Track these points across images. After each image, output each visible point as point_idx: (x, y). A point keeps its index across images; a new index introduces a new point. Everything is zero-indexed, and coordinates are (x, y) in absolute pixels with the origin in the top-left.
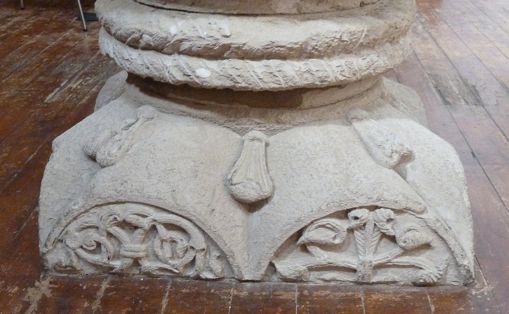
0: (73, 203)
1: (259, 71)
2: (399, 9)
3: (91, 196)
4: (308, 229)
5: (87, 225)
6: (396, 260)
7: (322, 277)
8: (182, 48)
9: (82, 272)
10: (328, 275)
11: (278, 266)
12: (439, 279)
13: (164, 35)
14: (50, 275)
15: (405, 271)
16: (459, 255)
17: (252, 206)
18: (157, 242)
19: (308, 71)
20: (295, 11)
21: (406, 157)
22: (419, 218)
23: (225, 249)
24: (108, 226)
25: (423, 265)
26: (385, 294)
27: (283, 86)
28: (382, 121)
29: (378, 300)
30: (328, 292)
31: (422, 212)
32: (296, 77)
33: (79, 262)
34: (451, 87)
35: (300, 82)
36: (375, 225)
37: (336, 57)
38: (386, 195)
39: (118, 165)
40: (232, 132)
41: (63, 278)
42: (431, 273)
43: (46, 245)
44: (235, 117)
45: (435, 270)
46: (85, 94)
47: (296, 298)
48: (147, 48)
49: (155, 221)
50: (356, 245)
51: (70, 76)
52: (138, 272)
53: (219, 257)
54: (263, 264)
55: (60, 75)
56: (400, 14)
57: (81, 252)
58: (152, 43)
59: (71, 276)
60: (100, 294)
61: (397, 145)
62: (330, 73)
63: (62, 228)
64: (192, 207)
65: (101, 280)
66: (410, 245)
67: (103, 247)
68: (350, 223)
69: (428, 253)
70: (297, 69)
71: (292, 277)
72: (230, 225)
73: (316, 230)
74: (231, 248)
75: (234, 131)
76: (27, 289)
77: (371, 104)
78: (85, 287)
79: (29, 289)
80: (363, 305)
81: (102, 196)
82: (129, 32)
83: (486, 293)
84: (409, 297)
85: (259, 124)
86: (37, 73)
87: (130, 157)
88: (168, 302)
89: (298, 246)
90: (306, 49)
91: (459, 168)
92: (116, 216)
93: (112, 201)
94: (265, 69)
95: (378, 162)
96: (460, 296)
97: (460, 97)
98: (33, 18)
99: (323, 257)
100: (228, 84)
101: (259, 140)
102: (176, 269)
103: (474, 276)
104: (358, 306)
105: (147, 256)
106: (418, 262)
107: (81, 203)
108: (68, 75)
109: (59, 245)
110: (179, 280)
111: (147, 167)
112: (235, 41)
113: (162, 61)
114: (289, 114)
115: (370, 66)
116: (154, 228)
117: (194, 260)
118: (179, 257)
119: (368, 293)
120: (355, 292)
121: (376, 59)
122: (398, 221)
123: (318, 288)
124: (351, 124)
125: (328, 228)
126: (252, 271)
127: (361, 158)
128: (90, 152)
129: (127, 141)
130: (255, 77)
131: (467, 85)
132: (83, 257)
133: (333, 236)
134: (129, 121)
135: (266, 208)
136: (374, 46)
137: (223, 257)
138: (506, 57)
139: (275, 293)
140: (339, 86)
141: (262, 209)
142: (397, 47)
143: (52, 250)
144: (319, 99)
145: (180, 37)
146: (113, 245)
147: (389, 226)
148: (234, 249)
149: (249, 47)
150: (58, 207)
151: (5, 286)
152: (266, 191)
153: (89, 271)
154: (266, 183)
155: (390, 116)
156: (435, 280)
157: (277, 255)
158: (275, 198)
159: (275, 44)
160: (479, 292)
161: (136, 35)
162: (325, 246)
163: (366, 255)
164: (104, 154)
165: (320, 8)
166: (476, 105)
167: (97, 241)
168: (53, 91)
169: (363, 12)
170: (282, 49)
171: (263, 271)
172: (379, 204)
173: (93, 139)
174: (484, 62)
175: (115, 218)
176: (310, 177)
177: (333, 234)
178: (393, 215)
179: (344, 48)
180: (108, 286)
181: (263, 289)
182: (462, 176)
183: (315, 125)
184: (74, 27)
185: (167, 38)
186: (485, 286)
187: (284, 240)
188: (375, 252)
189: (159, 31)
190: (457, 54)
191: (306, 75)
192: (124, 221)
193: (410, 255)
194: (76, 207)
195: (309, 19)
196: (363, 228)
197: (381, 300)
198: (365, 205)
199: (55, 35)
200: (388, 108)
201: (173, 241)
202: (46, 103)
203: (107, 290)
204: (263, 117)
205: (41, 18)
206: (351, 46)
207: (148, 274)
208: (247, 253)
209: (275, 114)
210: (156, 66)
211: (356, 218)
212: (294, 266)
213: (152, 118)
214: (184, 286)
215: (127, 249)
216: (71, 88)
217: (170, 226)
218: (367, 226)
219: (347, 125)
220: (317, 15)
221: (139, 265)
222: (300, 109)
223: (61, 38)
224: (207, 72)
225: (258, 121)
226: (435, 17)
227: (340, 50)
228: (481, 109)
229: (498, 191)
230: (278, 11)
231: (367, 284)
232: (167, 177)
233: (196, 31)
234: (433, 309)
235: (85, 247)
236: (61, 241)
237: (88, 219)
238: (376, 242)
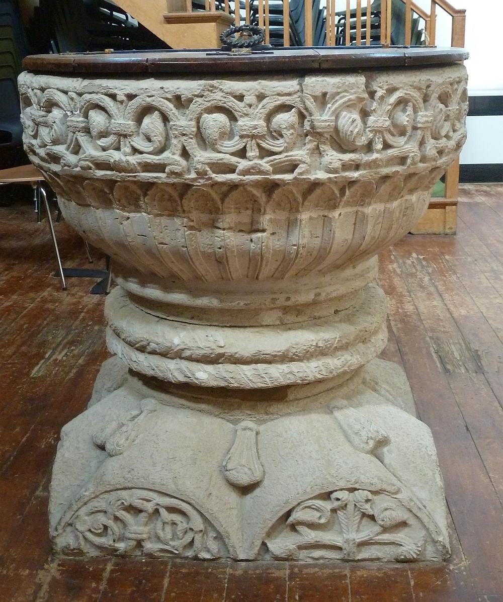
0: (84, 489)
1: (249, 374)
2: (369, 314)
3: (101, 483)
4: (295, 510)
5: (96, 509)
6: (377, 538)
7: (311, 556)
8: (183, 355)
9: (88, 554)
10: (317, 553)
11: (269, 545)
12: (418, 555)
14: (58, 558)
15: (387, 548)
16: (434, 532)
17: (245, 490)
18: (159, 524)
19: (291, 373)
20: (278, 322)
21: (382, 442)
22: (393, 498)
23: (221, 530)
24: (116, 510)
25: (403, 542)
26: (369, 570)
27: (270, 385)
28: (360, 408)
29: (362, 576)
30: (317, 569)
31: (396, 493)
32: (281, 377)
33: (85, 544)
34: (453, 352)
35: (284, 381)
36: (355, 505)
37: (315, 359)
38: (363, 478)
39: (125, 454)
40: (226, 422)
41: (71, 560)
42: (410, 549)
43: (56, 529)
44: (229, 409)
45: (414, 547)
46: (72, 367)
47: (287, 575)
48: (153, 353)
49: (158, 504)
50: (340, 524)
51: (54, 345)
52: (140, 554)
53: (215, 538)
54: (256, 544)
55: (43, 344)
56: (369, 318)
57: (89, 536)
58: (157, 350)
59: (77, 558)
60: (106, 575)
61: (372, 431)
62: (309, 373)
63: (73, 513)
64: (191, 492)
65: (105, 562)
66: (388, 523)
67: (109, 529)
68: (333, 503)
69: (406, 530)
70: (281, 371)
71: (283, 555)
72: (226, 509)
73: (303, 511)
74: (227, 529)
75: (228, 421)
76: (37, 571)
77: (352, 392)
78: (91, 569)
79: (39, 571)
80: (348, 581)
81: (112, 483)
82: (138, 340)
83: (463, 568)
84: (392, 573)
85: (250, 415)
86: (19, 342)
87: (136, 447)
88: (170, 581)
89: (287, 526)
90: (288, 355)
91: (432, 450)
92: (123, 501)
93: (120, 487)
94: (253, 372)
95: (356, 448)
96: (440, 572)
97: (461, 363)
98: (6, 273)
99: (311, 536)
100: (222, 384)
101: (250, 429)
102: (176, 550)
103: (450, 552)
104: (344, 582)
105: (149, 538)
106: (397, 539)
107: (92, 490)
108: (51, 344)
109: (69, 529)
110: (178, 561)
111: (151, 456)
112: (229, 350)
113: (166, 364)
114: (276, 405)
115: (345, 365)
116: (157, 511)
117: (192, 541)
118: (178, 539)
119: (353, 570)
120: (341, 569)
121: (349, 358)
122: (376, 501)
123: (307, 566)
124: (332, 412)
125: (314, 509)
126: (247, 551)
127: (341, 444)
128: (99, 442)
129: (133, 432)
130: (246, 379)
131: (469, 349)
132: (90, 540)
133: (319, 516)
134: (135, 413)
135: (257, 492)
136: (347, 347)
137: (219, 537)
139: (268, 572)
140: (320, 381)
141: (254, 492)
142: (369, 345)
143: (61, 534)
144: (302, 393)
145: (182, 347)
146: (119, 528)
147: (367, 506)
148: (230, 530)
149: (240, 355)
150: (67, 494)
151: (17, 569)
152: (257, 476)
153: (94, 553)
154: (257, 469)
155: (368, 402)
156: (415, 556)
157: (269, 534)
158: (266, 482)
159: (262, 353)
160: (456, 567)
161: (144, 343)
162: (312, 526)
163: (348, 534)
164: (114, 444)
165: (300, 319)
166: (476, 372)
167: (105, 524)
168: (38, 364)
169: (337, 319)
170: (267, 356)
171: (256, 550)
172: (357, 486)
173: (102, 430)
174: (490, 322)
175: (123, 503)
176: (296, 463)
177: (318, 514)
178: (370, 496)
179: (320, 352)
180: (112, 567)
181: (257, 568)
182: (434, 458)
183: (299, 415)
184: (52, 284)
185: (171, 347)
186: (463, 561)
187: (275, 520)
188: (358, 530)
189: (164, 341)
190: (463, 312)
191: (288, 376)
192: (130, 505)
193: (390, 533)
194: (87, 494)
195: (290, 329)
196: (345, 508)
197: (365, 576)
198: (345, 487)
199: (32, 295)
200: (370, 395)
201: (174, 524)
202: (33, 378)
203: (112, 571)
204: (254, 409)
205: (15, 274)
206: (327, 350)
207: (150, 555)
208: (241, 534)
209: (264, 406)
210: (161, 369)
211: (338, 499)
212: (284, 545)
213: (155, 411)
214: (183, 566)
215: (132, 532)
216: (56, 360)
217: (171, 510)
218: (348, 506)
219: (329, 414)
220: (296, 325)
221: (142, 547)
222: (286, 401)
223: (38, 299)
224: (204, 375)
225: (249, 412)
226: (444, 266)
227: (317, 354)
228: (481, 377)
229: (487, 467)
230: (264, 324)
231: (353, 561)
232: (169, 464)
233: (196, 342)
234: (412, 583)
235: (93, 530)
236: (71, 525)
237: (96, 504)
238: (357, 521)
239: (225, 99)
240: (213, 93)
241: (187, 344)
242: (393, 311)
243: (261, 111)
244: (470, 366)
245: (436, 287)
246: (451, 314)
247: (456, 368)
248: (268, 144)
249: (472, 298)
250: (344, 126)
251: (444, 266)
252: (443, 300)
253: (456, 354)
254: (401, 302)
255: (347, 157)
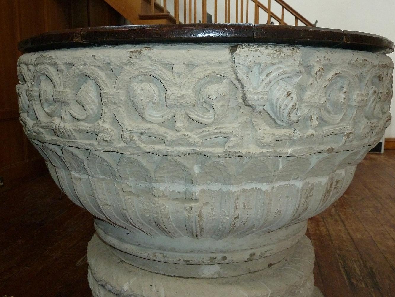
13: (119, 289)
97: (361, 279)
131: (365, 266)
138: (393, 239)
174: (378, 245)
189: (117, 285)
190: (359, 236)
226: (344, 201)
239: (153, 68)
240: (142, 61)
241: (134, 292)
242: (313, 232)
243: (190, 80)
244: (369, 281)
245: (339, 216)
246: (351, 236)
247: (359, 283)
248: (198, 116)
249: (363, 225)
250: (278, 100)
251: (344, 201)
252: (345, 226)
253: (357, 269)
254: (318, 226)
255: (281, 132)
